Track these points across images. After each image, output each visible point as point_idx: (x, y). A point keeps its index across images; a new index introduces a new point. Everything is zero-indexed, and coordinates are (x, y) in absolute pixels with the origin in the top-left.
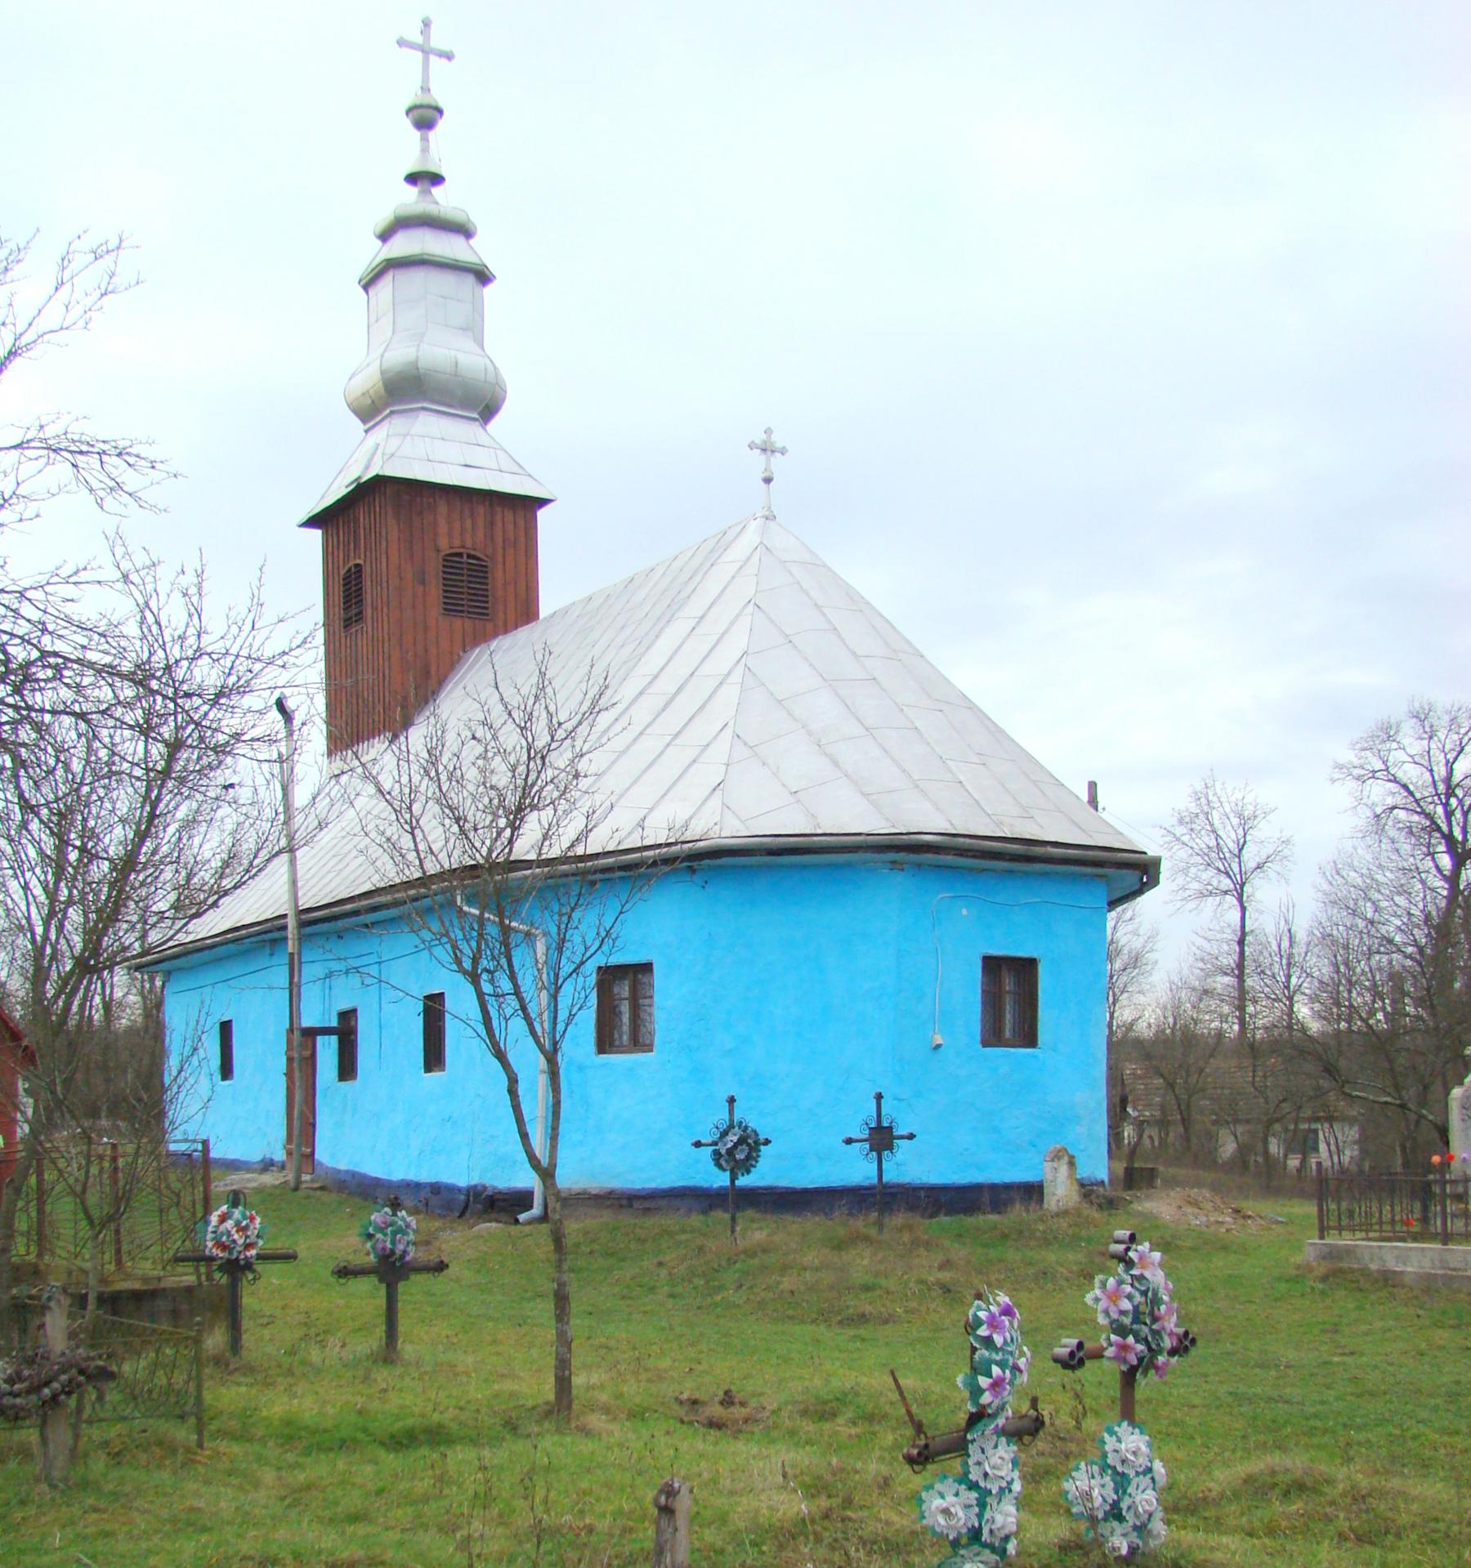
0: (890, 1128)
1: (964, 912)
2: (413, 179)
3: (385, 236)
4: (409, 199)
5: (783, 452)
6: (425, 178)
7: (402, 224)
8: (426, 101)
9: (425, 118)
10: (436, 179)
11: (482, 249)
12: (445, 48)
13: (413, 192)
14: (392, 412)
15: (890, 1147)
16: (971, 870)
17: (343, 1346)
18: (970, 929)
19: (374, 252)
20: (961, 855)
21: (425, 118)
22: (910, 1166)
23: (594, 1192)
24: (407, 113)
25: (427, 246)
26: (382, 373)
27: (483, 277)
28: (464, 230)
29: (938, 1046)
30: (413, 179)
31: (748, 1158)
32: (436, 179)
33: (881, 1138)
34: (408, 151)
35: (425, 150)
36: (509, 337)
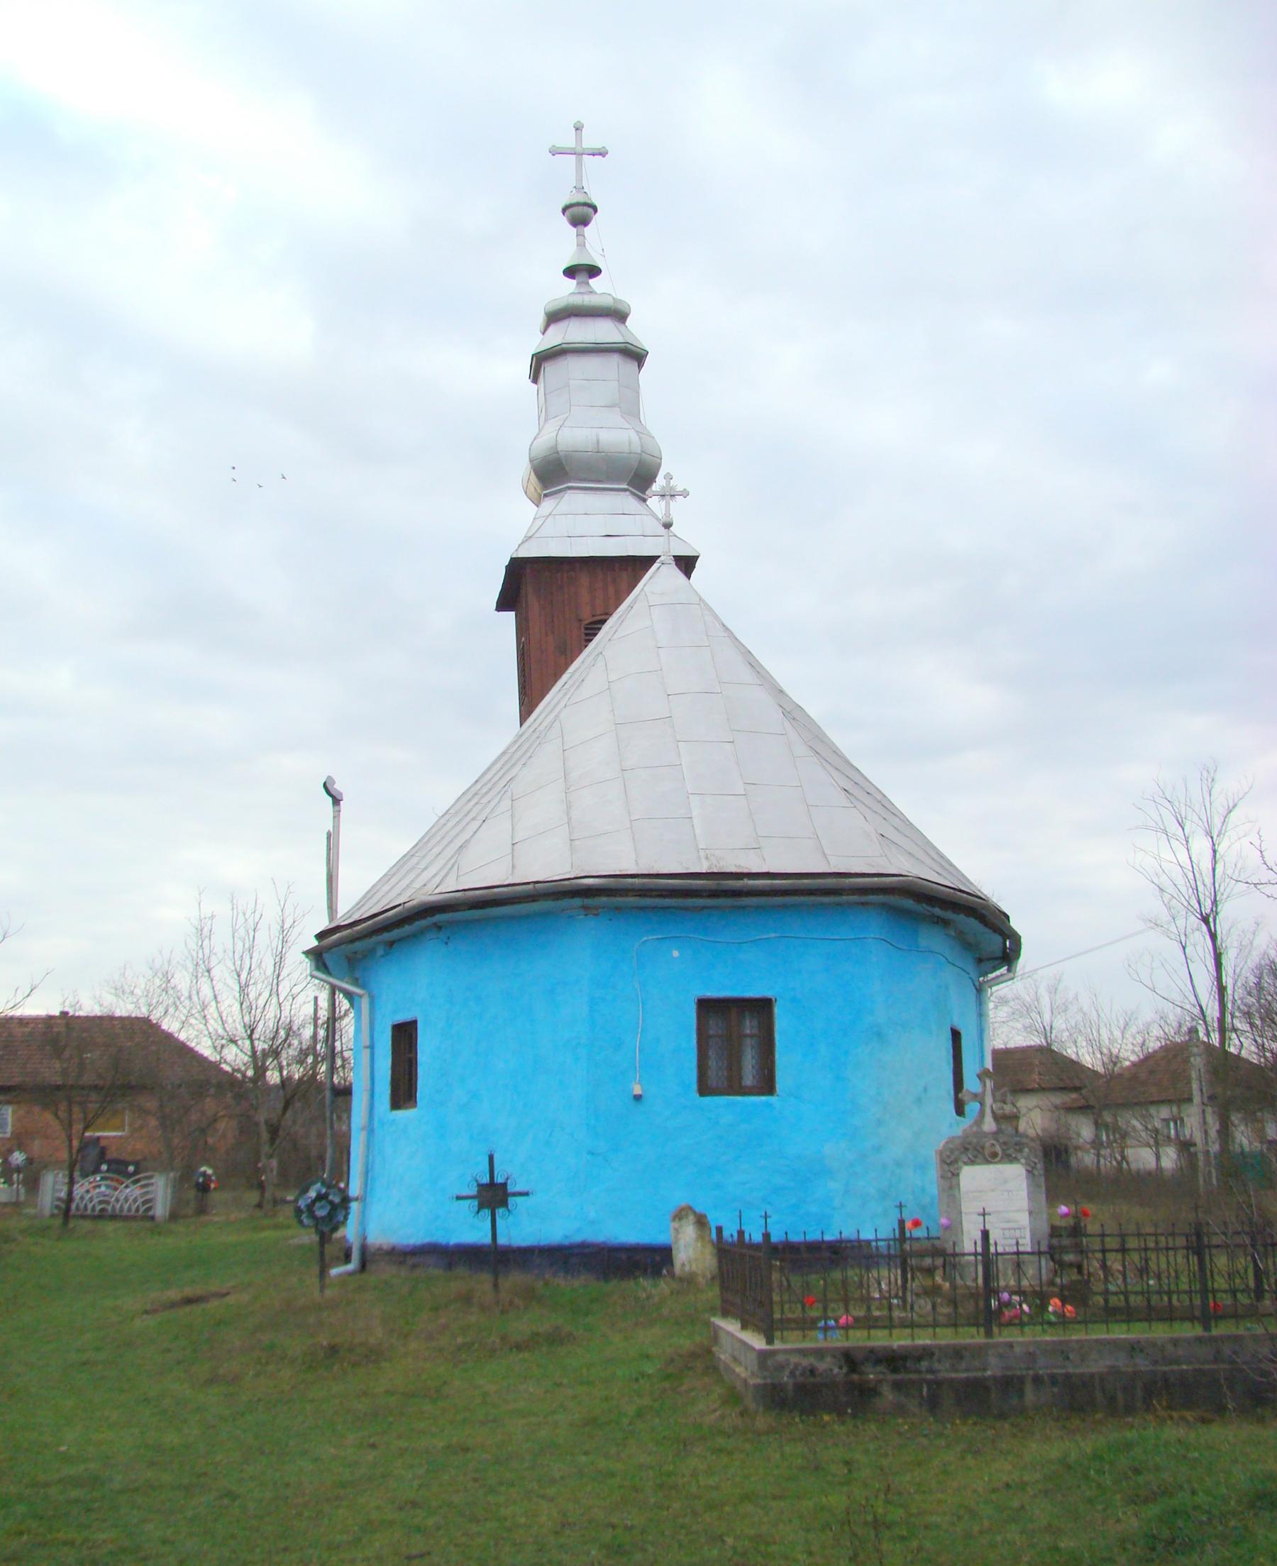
0: (504, 1185)
1: (676, 954)
2: (571, 272)
3: (554, 317)
4: (566, 291)
5: (685, 494)
6: (582, 271)
7: (554, 317)
8: (581, 199)
9: (580, 214)
10: (593, 271)
11: (638, 330)
12: (596, 145)
13: (571, 284)
14: (570, 488)
15: (504, 1203)
16: (654, 908)
17: (559, 1385)
18: (675, 977)
19: (538, 342)
20: (645, 896)
21: (580, 214)
22: (522, 1227)
23: (385, 1247)
24: (564, 211)
25: (587, 334)
26: (531, 461)
27: (636, 356)
28: (618, 315)
29: (638, 1098)
30: (571, 272)
31: (331, 1216)
32: (593, 271)
33: (493, 1195)
34: (564, 245)
35: (581, 245)
36: (669, 411)
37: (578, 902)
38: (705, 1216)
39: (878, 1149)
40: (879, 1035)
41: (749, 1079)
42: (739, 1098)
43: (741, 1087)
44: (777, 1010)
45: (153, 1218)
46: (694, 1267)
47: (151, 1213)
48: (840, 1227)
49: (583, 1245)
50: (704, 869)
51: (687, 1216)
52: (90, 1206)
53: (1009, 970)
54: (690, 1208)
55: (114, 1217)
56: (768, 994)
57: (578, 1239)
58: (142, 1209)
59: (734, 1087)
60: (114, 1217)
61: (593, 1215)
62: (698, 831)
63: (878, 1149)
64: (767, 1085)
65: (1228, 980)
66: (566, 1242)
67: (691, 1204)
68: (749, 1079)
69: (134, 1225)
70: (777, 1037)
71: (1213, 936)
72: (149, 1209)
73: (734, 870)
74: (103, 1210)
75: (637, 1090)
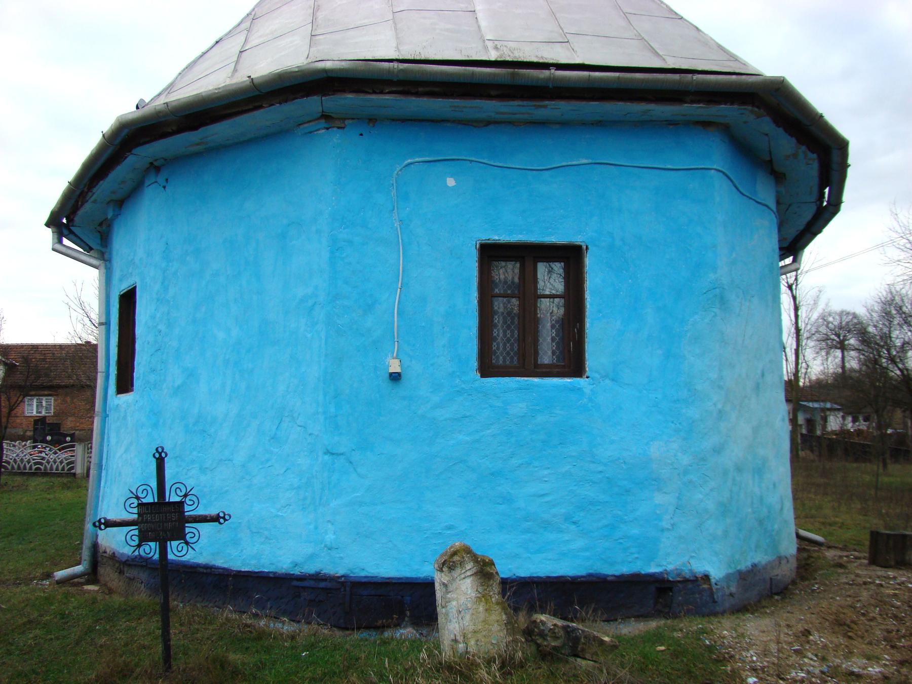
1: (451, 182)
18: (445, 214)
29: (395, 377)
37: (313, 104)
38: (491, 563)
39: (718, 450)
40: (723, 301)
41: (546, 356)
42: (536, 380)
43: (536, 365)
44: (589, 261)
45: (74, 474)
46: (472, 647)
47: (73, 471)
48: (666, 560)
49: (317, 577)
50: (493, 56)
51: (462, 564)
52: (28, 466)
53: (794, 261)
54: (468, 551)
55: (45, 474)
56: (577, 239)
57: (310, 568)
58: (66, 469)
59: (526, 365)
60: (45, 474)
61: (330, 537)
62: (483, 23)
63: (718, 450)
64: (572, 363)
65: (801, 325)
66: (296, 571)
67: (468, 543)
68: (546, 356)
69: (57, 481)
70: (588, 296)
71: (794, 298)
72: (72, 468)
73: (535, 60)
74: (37, 469)
75: (395, 367)
